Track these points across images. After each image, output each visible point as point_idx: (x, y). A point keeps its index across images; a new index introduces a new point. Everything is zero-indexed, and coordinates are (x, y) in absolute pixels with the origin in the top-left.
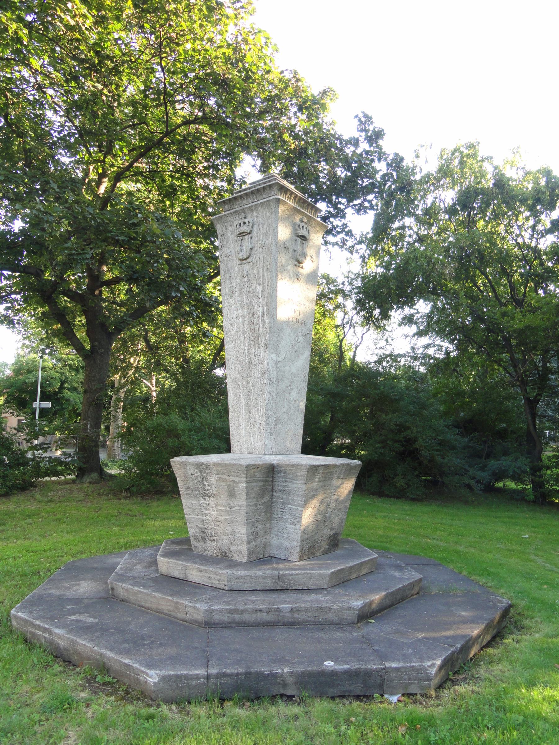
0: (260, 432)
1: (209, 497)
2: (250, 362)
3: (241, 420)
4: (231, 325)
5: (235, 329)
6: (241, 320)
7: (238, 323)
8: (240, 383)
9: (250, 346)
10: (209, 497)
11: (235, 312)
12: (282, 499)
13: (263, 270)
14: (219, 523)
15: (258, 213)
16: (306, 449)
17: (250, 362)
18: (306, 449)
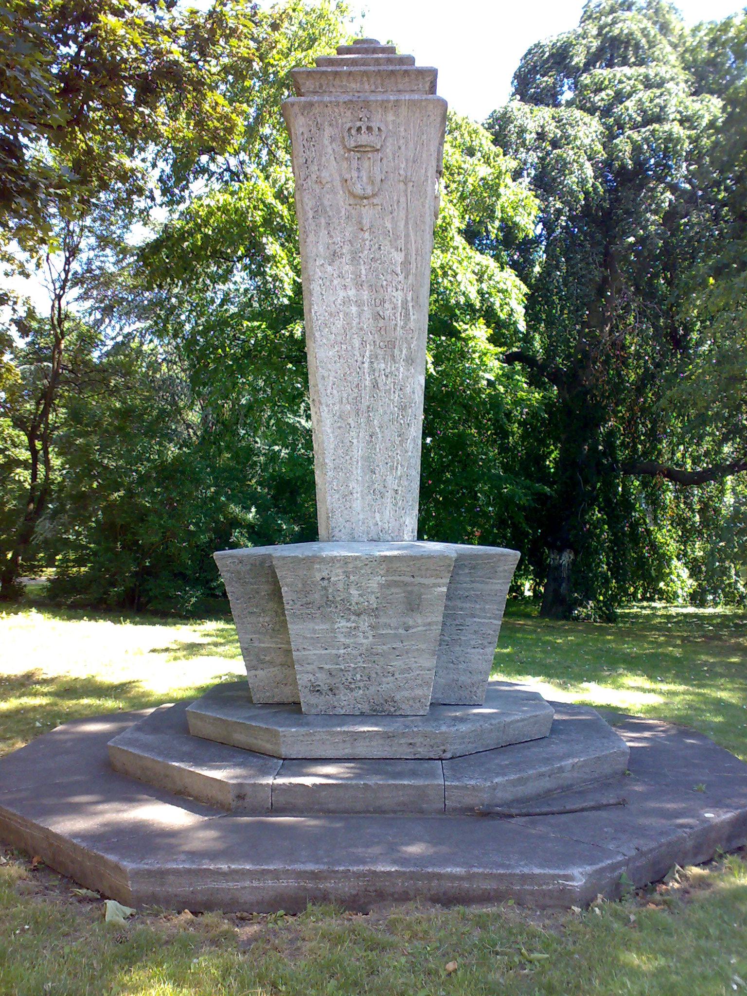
0: (395, 505)
1: (359, 615)
2: (375, 385)
3: (352, 485)
4: (331, 314)
5: (339, 324)
6: (354, 309)
7: (346, 314)
8: (350, 421)
9: (374, 357)
10: (359, 615)
11: (342, 294)
12: (461, 609)
13: (407, 223)
14: (376, 658)
15: (398, 116)
16: (428, 529)
17: (375, 385)
18: (428, 529)
